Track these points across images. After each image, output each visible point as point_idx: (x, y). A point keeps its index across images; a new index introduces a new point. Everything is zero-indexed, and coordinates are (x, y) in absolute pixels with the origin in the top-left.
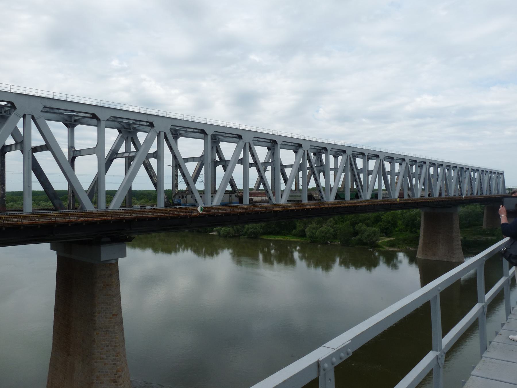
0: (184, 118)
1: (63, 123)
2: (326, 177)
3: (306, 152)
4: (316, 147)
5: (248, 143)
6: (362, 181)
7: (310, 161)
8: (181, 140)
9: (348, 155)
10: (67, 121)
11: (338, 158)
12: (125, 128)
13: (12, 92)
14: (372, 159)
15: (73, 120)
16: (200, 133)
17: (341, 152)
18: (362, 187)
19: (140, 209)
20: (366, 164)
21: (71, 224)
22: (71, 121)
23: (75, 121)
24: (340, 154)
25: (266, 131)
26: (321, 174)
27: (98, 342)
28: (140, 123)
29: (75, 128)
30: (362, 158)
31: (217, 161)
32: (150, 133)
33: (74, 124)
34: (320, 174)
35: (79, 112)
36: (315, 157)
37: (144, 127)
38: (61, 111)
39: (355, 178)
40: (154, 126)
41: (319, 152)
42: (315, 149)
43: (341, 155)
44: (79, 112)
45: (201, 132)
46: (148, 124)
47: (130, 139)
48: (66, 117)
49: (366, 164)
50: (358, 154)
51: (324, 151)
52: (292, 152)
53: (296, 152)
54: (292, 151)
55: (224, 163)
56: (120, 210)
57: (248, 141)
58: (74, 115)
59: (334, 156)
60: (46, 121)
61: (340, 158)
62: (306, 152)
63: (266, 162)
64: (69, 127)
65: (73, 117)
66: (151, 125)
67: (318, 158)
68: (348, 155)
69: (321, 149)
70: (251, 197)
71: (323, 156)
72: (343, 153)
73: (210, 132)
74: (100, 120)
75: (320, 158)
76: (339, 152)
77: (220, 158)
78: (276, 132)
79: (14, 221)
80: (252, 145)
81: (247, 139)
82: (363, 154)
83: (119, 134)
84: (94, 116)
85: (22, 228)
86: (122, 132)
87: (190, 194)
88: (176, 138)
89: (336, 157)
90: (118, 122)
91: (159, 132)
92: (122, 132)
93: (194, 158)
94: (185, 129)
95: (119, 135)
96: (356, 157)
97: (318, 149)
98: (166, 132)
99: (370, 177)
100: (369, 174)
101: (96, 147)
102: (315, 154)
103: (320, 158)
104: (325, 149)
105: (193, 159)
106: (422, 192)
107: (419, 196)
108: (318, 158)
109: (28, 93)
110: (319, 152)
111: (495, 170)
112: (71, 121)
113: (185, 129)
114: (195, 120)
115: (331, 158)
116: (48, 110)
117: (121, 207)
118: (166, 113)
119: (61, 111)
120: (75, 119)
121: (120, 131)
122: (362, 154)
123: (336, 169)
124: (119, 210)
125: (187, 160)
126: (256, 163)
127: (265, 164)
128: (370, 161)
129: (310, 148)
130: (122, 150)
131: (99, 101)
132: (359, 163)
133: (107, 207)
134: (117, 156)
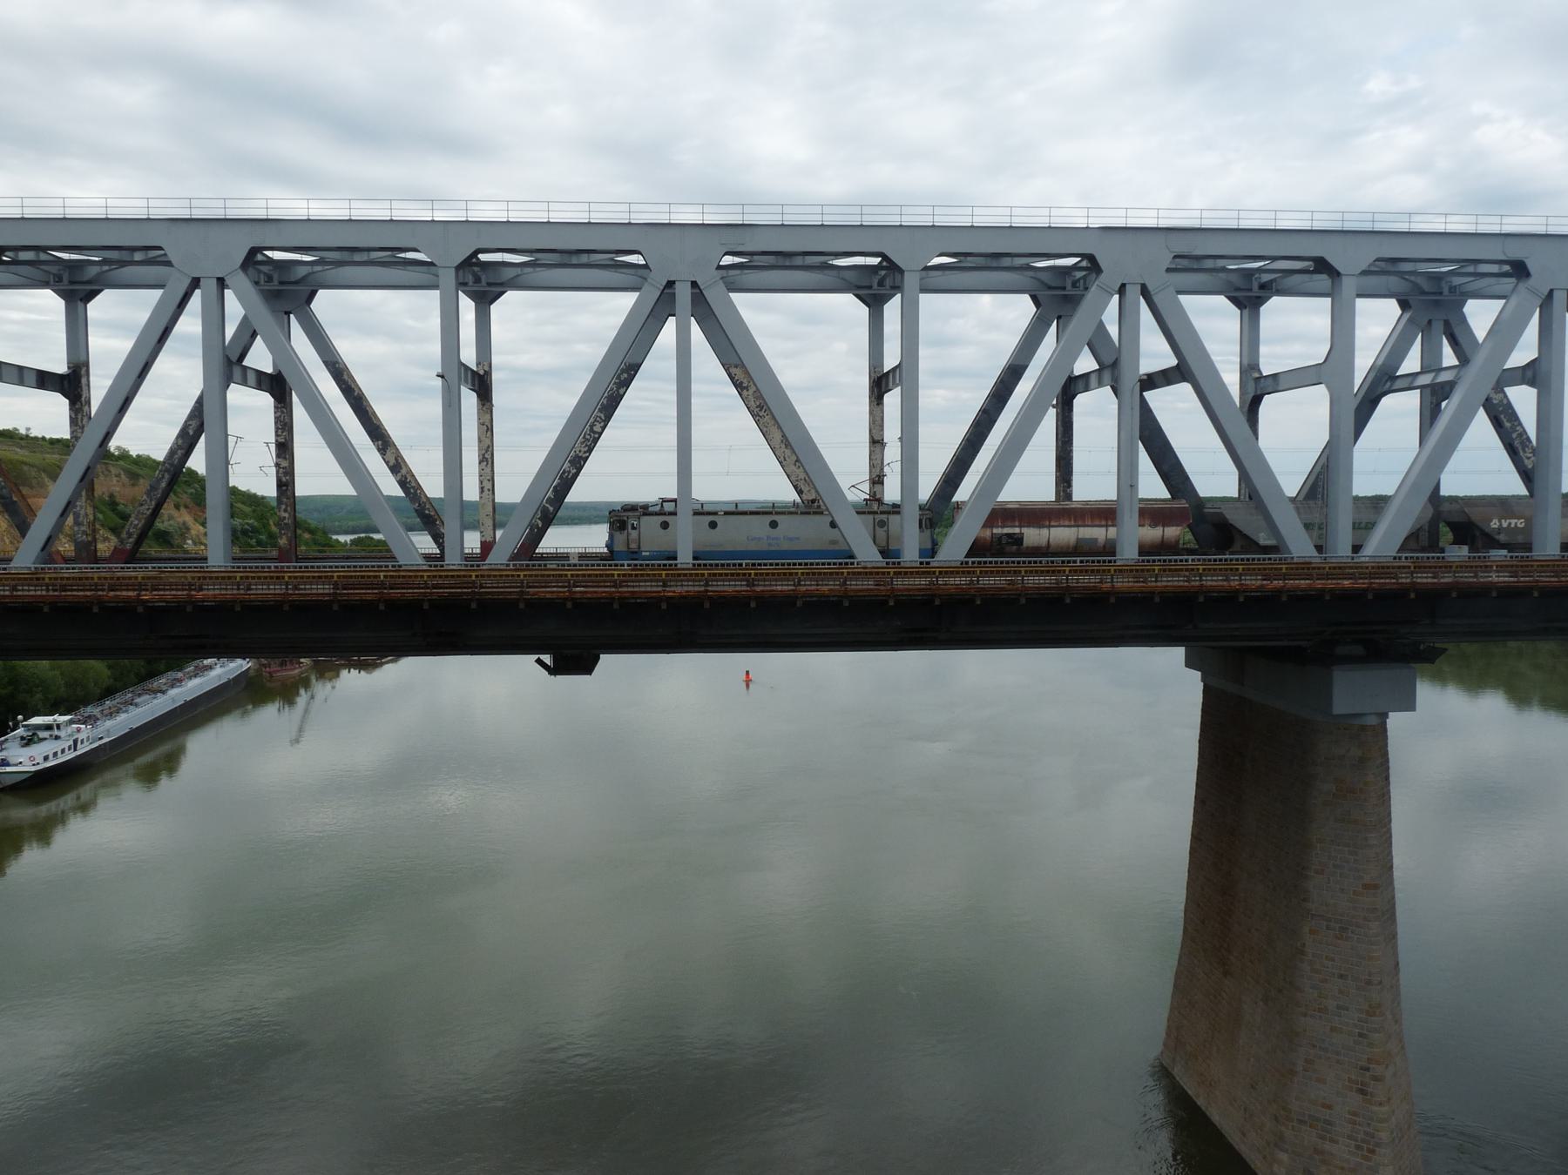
12: (1050, 288)
15: (1255, 286)
19: (1469, 558)
23: (1263, 287)
32: (1514, 300)
33: (1259, 297)
35: (1274, 259)
37: (1492, 280)
38: (1220, 263)
44: (1274, 259)
58: (1259, 270)
64: (1246, 308)
65: (1257, 276)
66: (1519, 270)
74: (1338, 274)
79: (953, 582)
83: (1400, 312)
84: (1322, 266)
86: (1410, 307)
92: (1410, 307)
95: (1402, 315)
98: (1150, 288)
113: (1470, 269)
116: (781, 261)
119: (1220, 263)
121: (1404, 305)
124: (1395, 558)
130: (1411, 363)
131: (1339, 216)
133: (1356, 548)
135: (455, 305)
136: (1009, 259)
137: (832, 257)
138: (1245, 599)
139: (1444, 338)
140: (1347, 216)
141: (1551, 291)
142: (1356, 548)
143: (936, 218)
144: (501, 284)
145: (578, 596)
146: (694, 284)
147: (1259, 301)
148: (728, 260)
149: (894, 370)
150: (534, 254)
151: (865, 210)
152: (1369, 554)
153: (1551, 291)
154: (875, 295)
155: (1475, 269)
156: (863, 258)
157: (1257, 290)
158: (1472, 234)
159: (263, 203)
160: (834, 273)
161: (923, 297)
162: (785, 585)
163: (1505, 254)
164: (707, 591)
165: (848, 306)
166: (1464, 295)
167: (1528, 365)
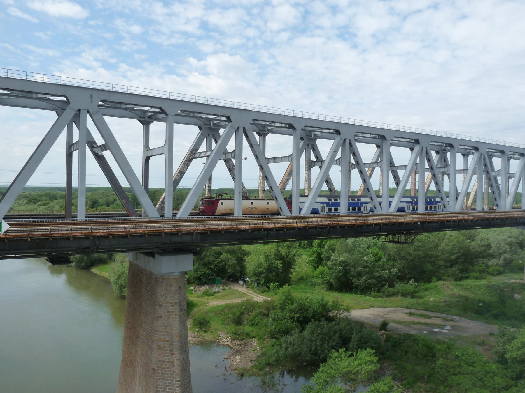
0: (266, 110)
1: (138, 120)
2: (453, 180)
3: (483, 155)
4: (439, 144)
5: (242, 128)
6: (500, 186)
7: (429, 160)
8: (270, 138)
9: (481, 154)
10: (140, 117)
11: (469, 157)
13: (9, 77)
14: (514, 158)
15: (146, 117)
16: (288, 128)
17: (473, 150)
18: (500, 193)
20: (506, 165)
21: (196, 232)
22: (144, 118)
23: (149, 117)
24: (471, 152)
25: (373, 125)
26: (446, 177)
27: (162, 382)
28: (220, 118)
29: (150, 125)
30: (501, 158)
31: (313, 161)
32: (227, 129)
33: (148, 121)
34: (350, 171)
35: (218, 116)
36: (438, 156)
37: (279, 129)
38: (200, 115)
39: (492, 181)
40: (231, 121)
41: (443, 150)
42: (407, 142)
43: (473, 153)
44: (218, 116)
45: (379, 137)
46: (287, 126)
47: (310, 146)
48: (59, 104)
49: (506, 165)
50: (495, 152)
51: (449, 148)
52: (408, 149)
53: (412, 150)
54: (408, 148)
55: (320, 164)
56: (190, 218)
57: (348, 137)
58: (214, 119)
59: (464, 155)
60: (104, 117)
61: (471, 157)
62: (483, 155)
63: (374, 162)
64: (261, 136)
65: (147, 113)
66: (338, 132)
67: (442, 157)
68: (481, 154)
69: (446, 146)
70: (426, 206)
71: (449, 155)
72: (475, 151)
73: (298, 126)
75: (445, 157)
76: (469, 150)
77: (317, 157)
78: (459, 136)
80: (428, 149)
81: (346, 134)
82: (502, 152)
84: (291, 126)
85: (223, 232)
86: (303, 140)
87: (274, 200)
88: (263, 134)
89: (465, 155)
90: (197, 118)
91: (237, 128)
92: (303, 140)
93: (282, 157)
94: (273, 125)
96: (493, 155)
97: (442, 146)
98: (246, 128)
99: (511, 181)
100: (509, 178)
101: (164, 146)
102: (437, 153)
103: (445, 157)
104: (451, 145)
105: (281, 159)
106: (291, 193)
107: (508, 207)
108: (442, 157)
109: (171, 97)
110: (443, 150)
111: (521, 147)
112: (211, 125)
113: (273, 125)
114: (258, 109)
115: (459, 157)
116: (25, 94)
117: (189, 216)
118: (387, 125)
119: (200, 115)
120: (149, 115)
121: (200, 128)
122: (502, 151)
123: (465, 171)
125: (275, 160)
126: (358, 164)
127: (372, 165)
128: (512, 161)
129: (251, 124)
130: (203, 148)
132: (497, 162)
133: (174, 215)
134: (194, 156)
135: (96, 121)
136: (35, 95)
137: (50, 96)
138: (210, 233)
139: (213, 139)
140: (427, 131)
141: (345, 139)
142: (174, 215)
143: (28, 77)
144: (219, 126)
145: (95, 234)
146: (426, 148)
147: (265, 135)
148: (100, 103)
149: (76, 143)
150: (12, 91)
151: (266, 108)
152: (179, 216)
153: (345, 139)
154: (210, 128)
155: (220, 118)
156: (62, 97)
157: (147, 118)
158: (339, 123)
159: (353, 120)
160: (52, 102)
161: (457, 154)
162: (259, 224)
163: (223, 113)
164: (51, 234)
165: (136, 125)
166: (317, 137)
167: (233, 151)
